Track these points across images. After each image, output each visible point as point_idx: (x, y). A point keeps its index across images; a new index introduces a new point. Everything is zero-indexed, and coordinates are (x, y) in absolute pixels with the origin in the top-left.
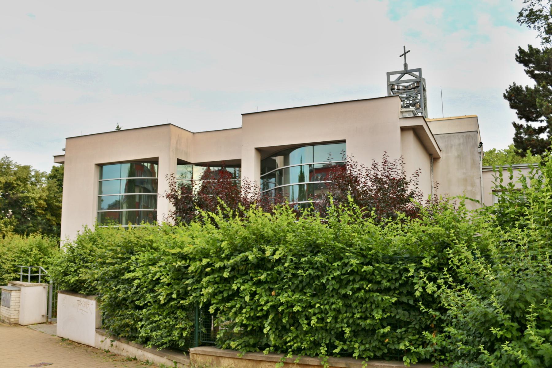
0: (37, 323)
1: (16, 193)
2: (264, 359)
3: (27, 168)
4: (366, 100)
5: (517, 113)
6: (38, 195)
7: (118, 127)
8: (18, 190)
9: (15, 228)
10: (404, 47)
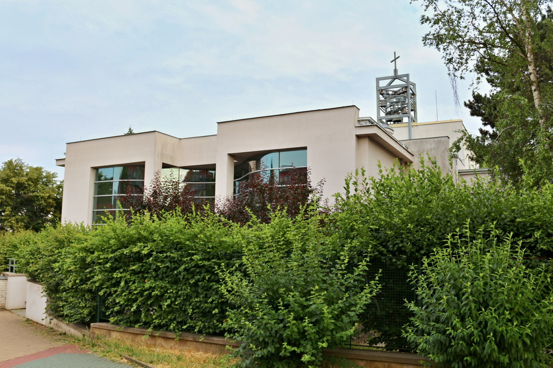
0: (20, 308)
1: (28, 193)
2: (139, 333)
3: (39, 170)
4: (343, 107)
5: (482, 120)
6: (47, 195)
7: (130, 129)
8: (29, 190)
9: (25, 224)
10: (395, 53)
